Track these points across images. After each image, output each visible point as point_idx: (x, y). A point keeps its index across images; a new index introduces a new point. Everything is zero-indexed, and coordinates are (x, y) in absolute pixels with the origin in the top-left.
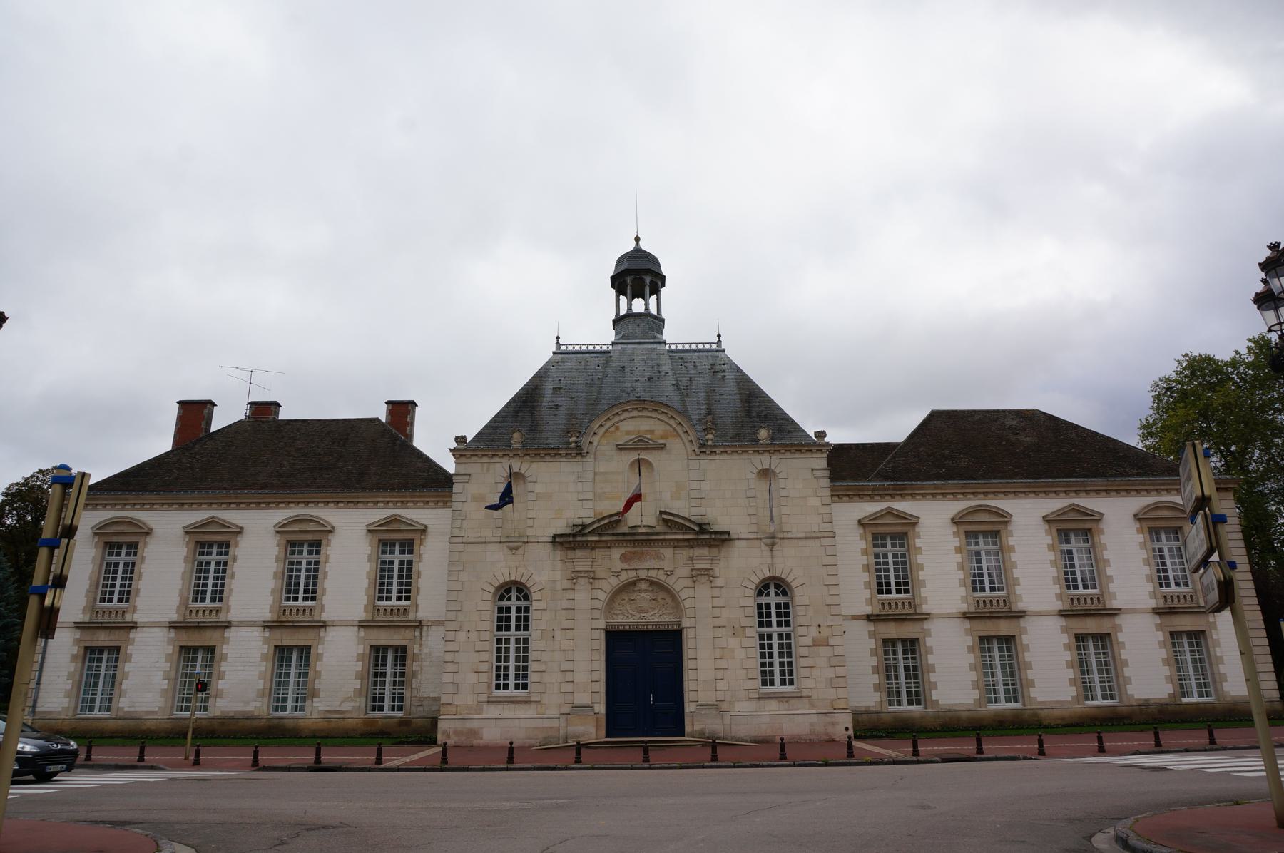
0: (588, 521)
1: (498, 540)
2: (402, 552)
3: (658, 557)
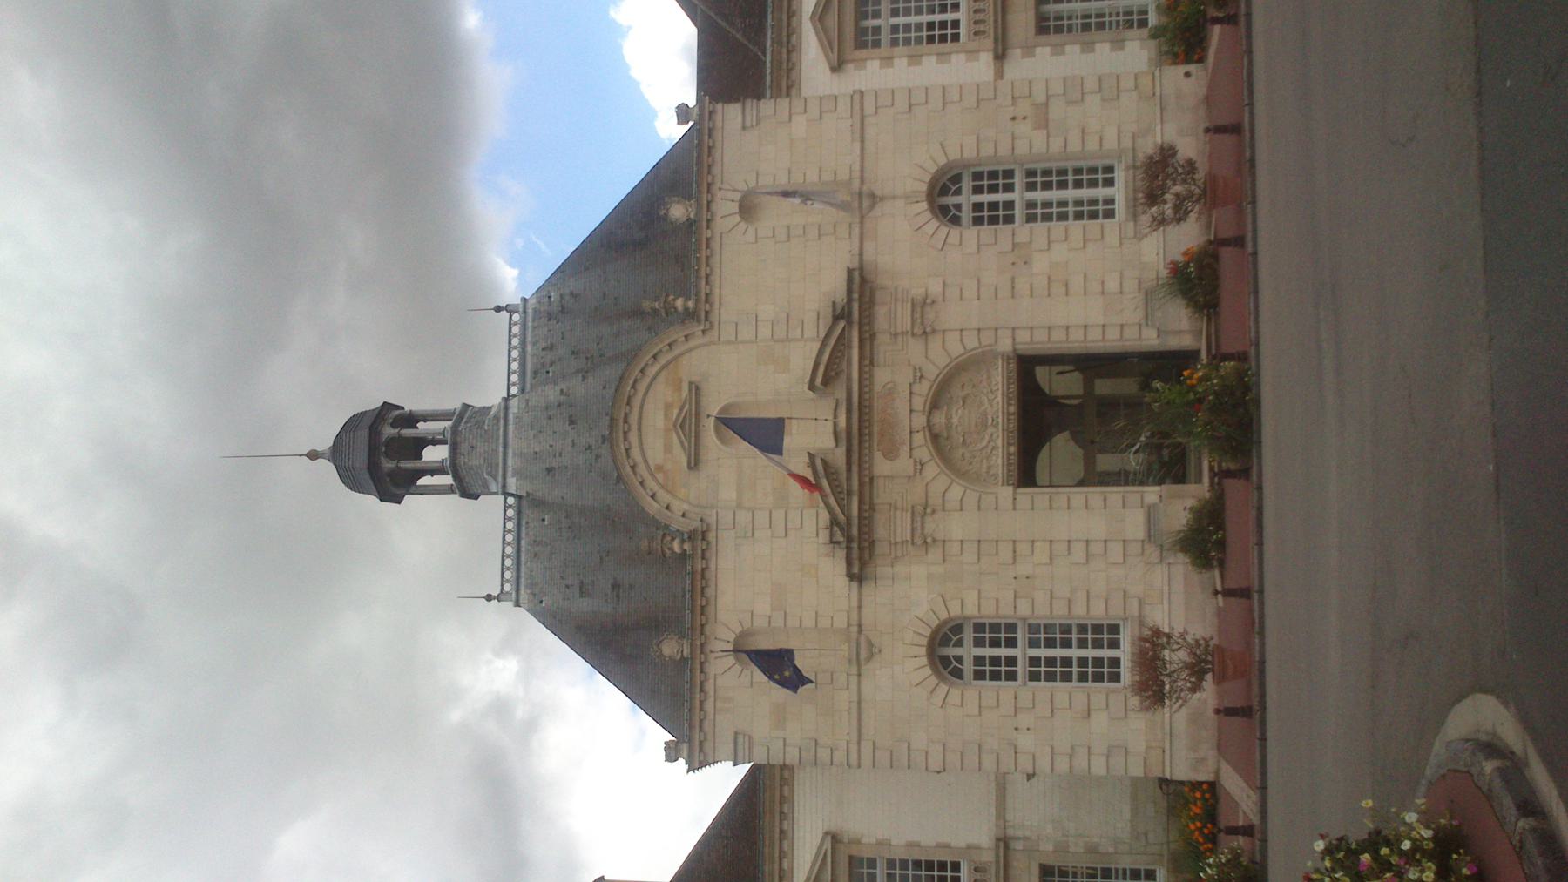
0: (825, 517)
1: (854, 680)
3: (891, 392)
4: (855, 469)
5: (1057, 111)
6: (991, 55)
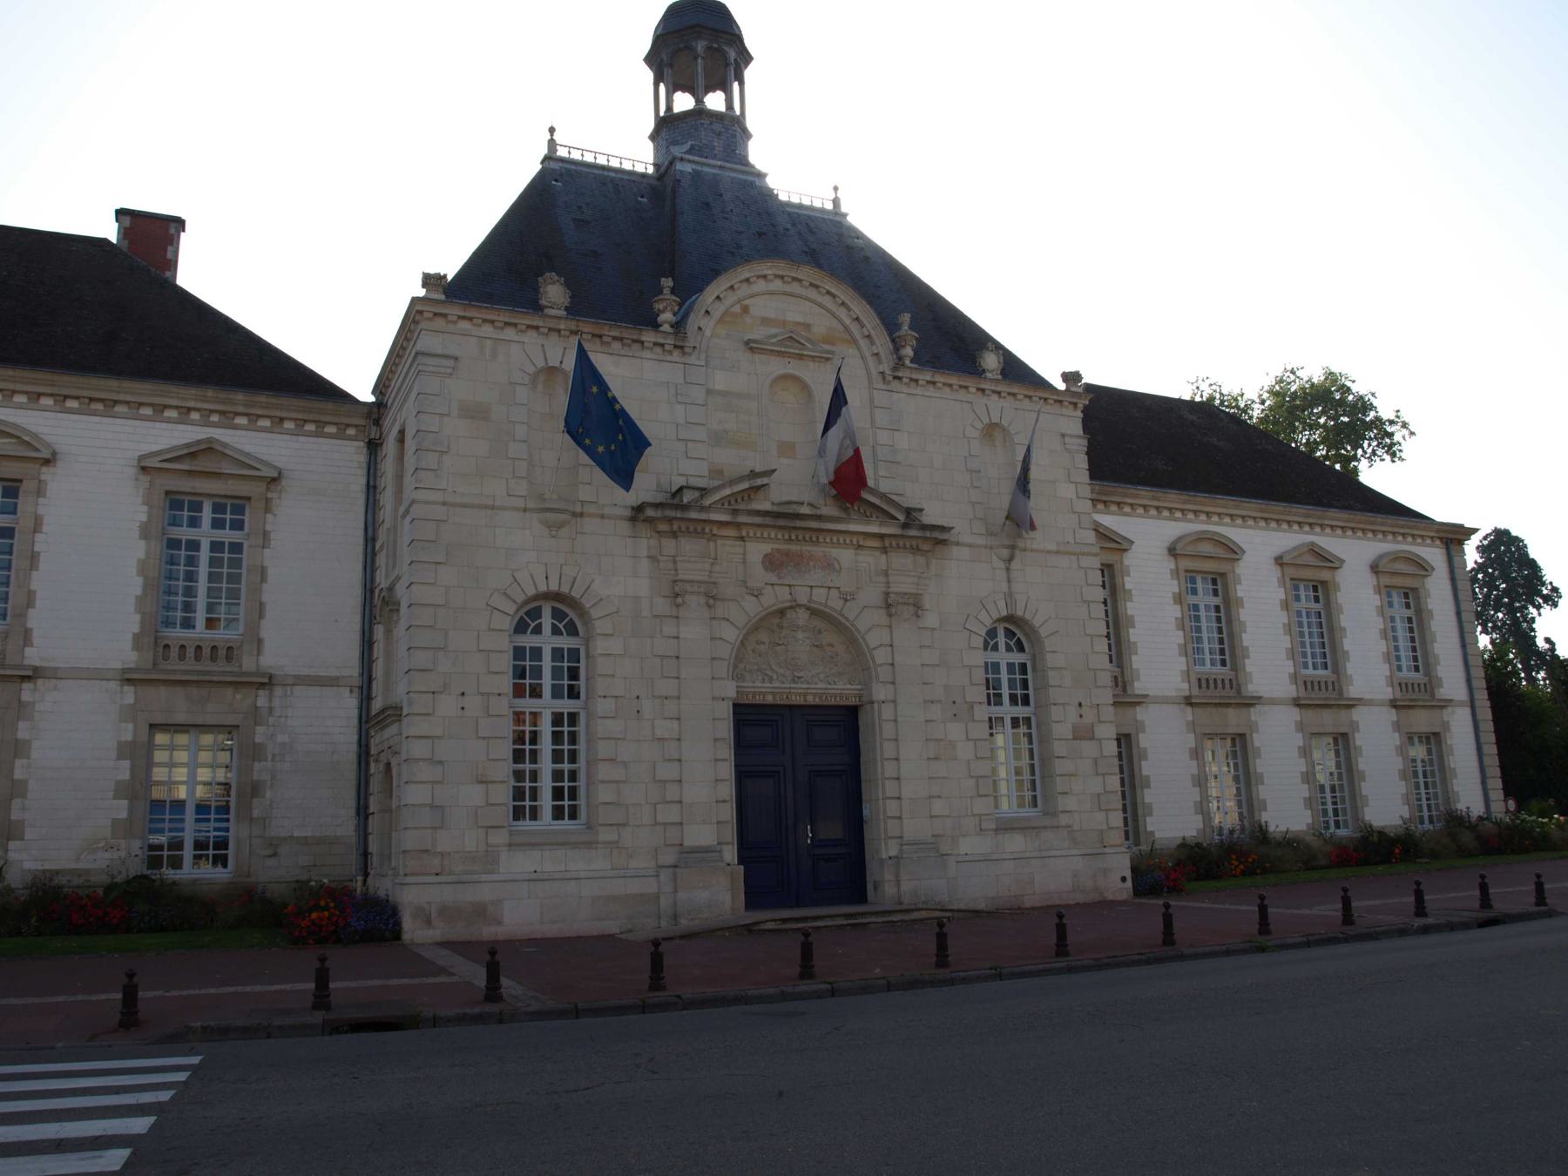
1: (520, 503)
2: (217, 524)
4: (758, 520)
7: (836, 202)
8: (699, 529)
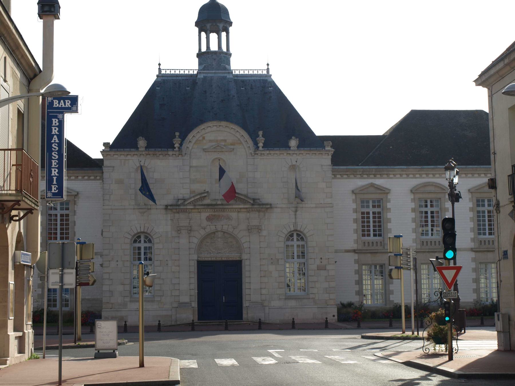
0: (187, 196)
5: (323, 272)
6: (356, 248)
7: (268, 70)
8: (185, 211)
